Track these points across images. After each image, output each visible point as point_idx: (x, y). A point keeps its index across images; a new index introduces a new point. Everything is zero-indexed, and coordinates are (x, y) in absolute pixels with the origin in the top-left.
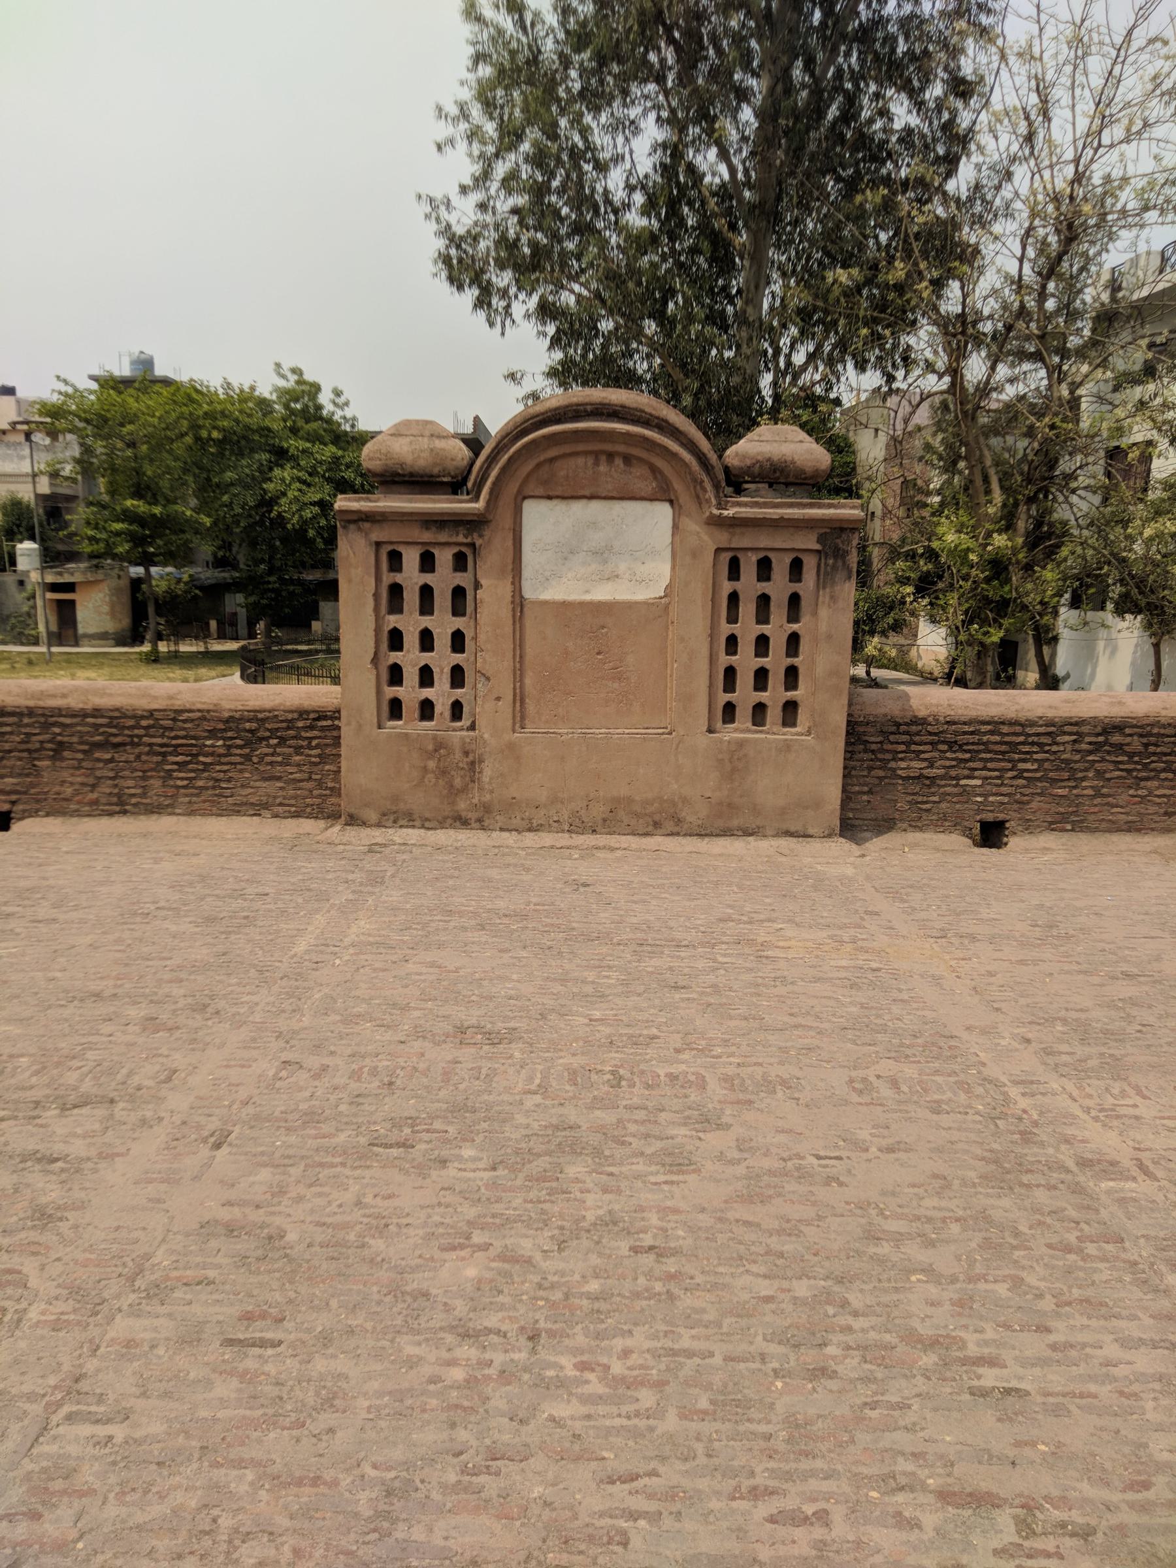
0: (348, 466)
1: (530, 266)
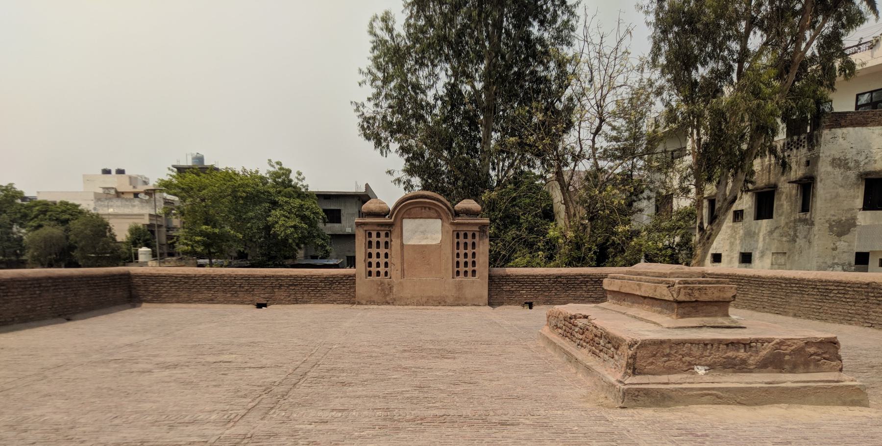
0: (307, 209)
1: (398, 130)
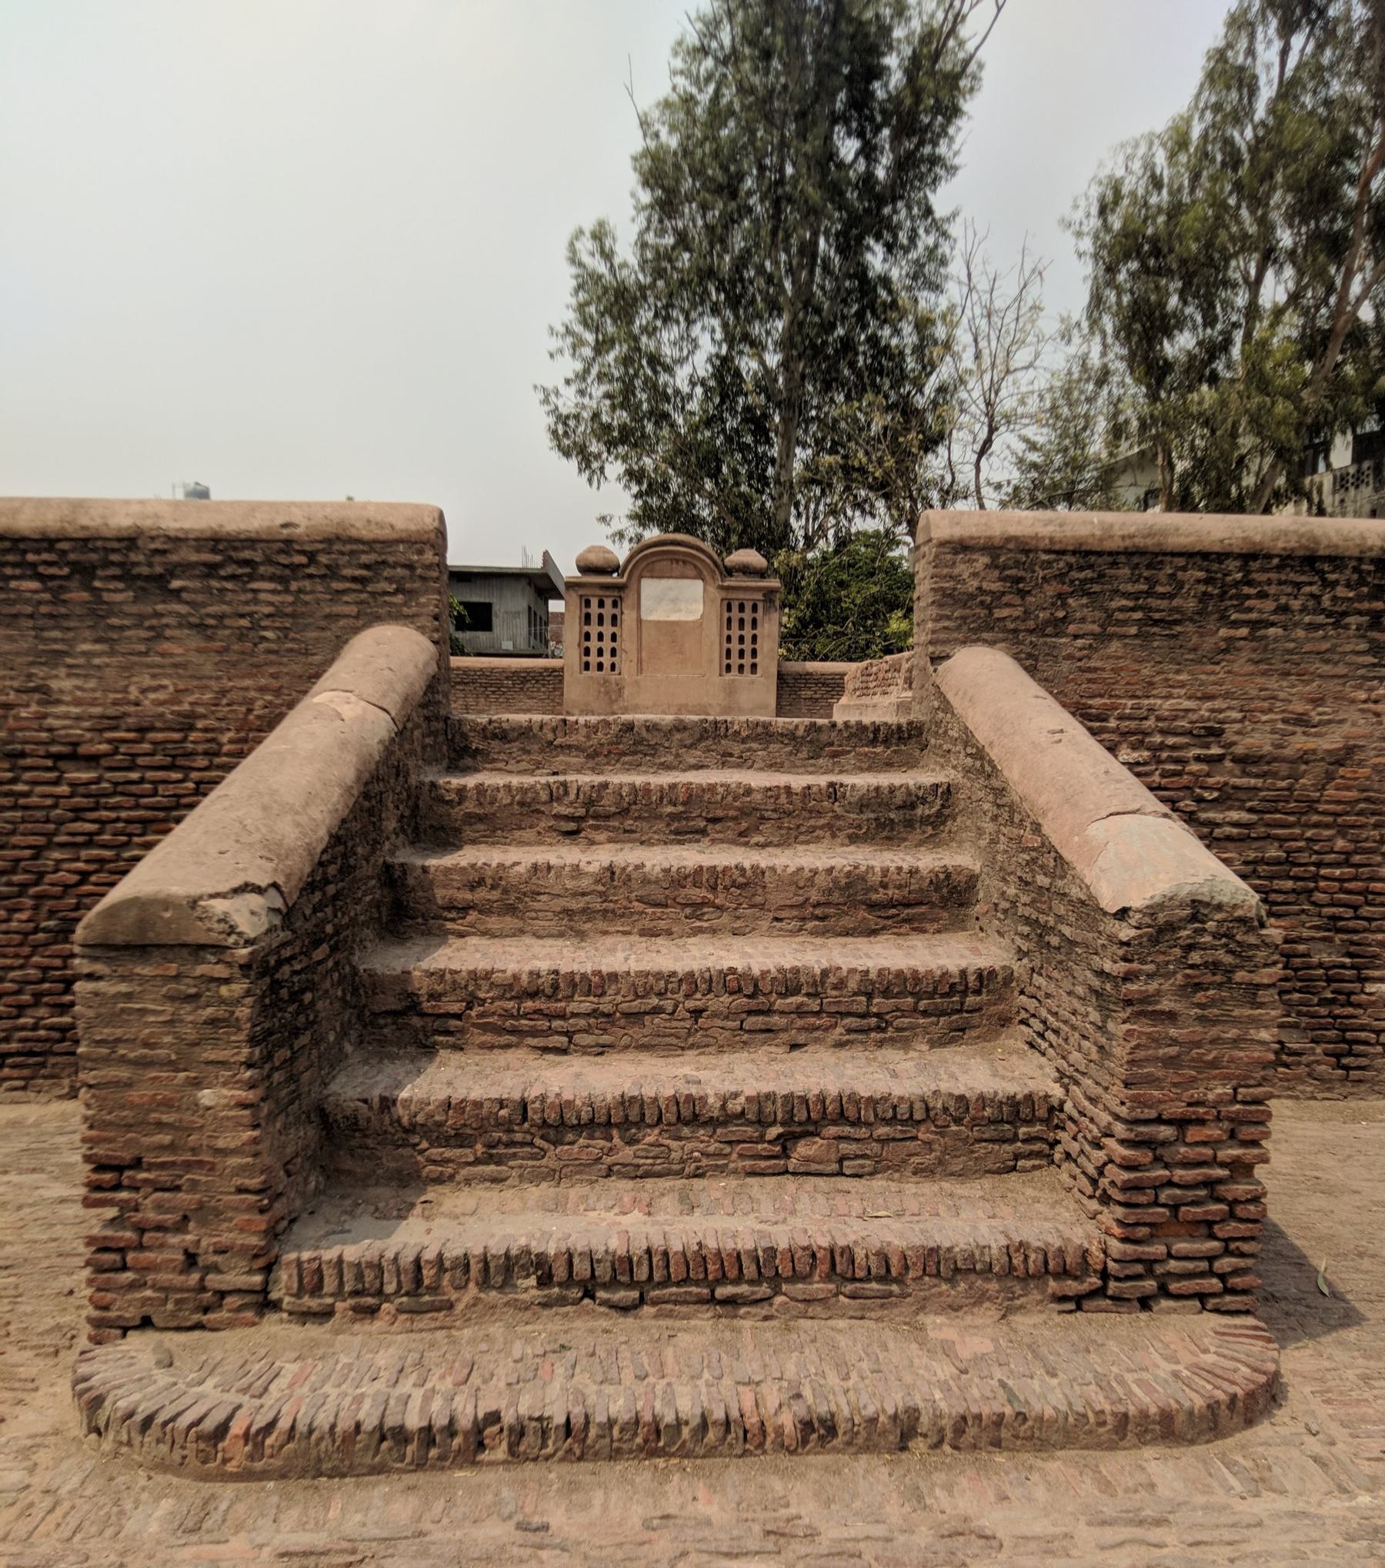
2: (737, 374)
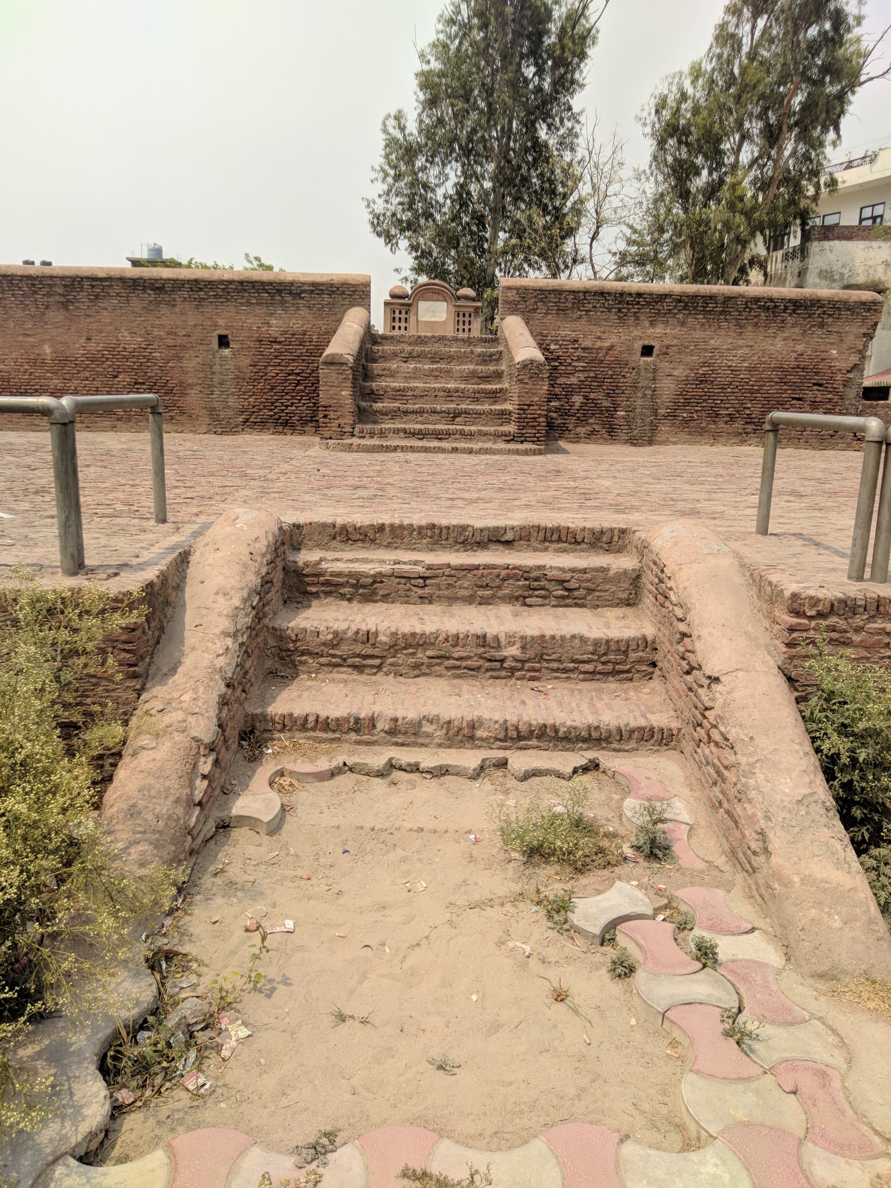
1: (410, 226)
2: (469, 193)
